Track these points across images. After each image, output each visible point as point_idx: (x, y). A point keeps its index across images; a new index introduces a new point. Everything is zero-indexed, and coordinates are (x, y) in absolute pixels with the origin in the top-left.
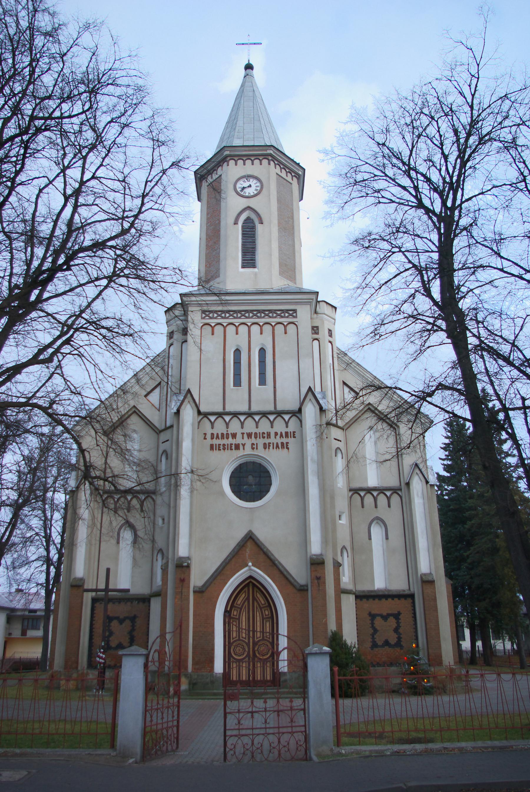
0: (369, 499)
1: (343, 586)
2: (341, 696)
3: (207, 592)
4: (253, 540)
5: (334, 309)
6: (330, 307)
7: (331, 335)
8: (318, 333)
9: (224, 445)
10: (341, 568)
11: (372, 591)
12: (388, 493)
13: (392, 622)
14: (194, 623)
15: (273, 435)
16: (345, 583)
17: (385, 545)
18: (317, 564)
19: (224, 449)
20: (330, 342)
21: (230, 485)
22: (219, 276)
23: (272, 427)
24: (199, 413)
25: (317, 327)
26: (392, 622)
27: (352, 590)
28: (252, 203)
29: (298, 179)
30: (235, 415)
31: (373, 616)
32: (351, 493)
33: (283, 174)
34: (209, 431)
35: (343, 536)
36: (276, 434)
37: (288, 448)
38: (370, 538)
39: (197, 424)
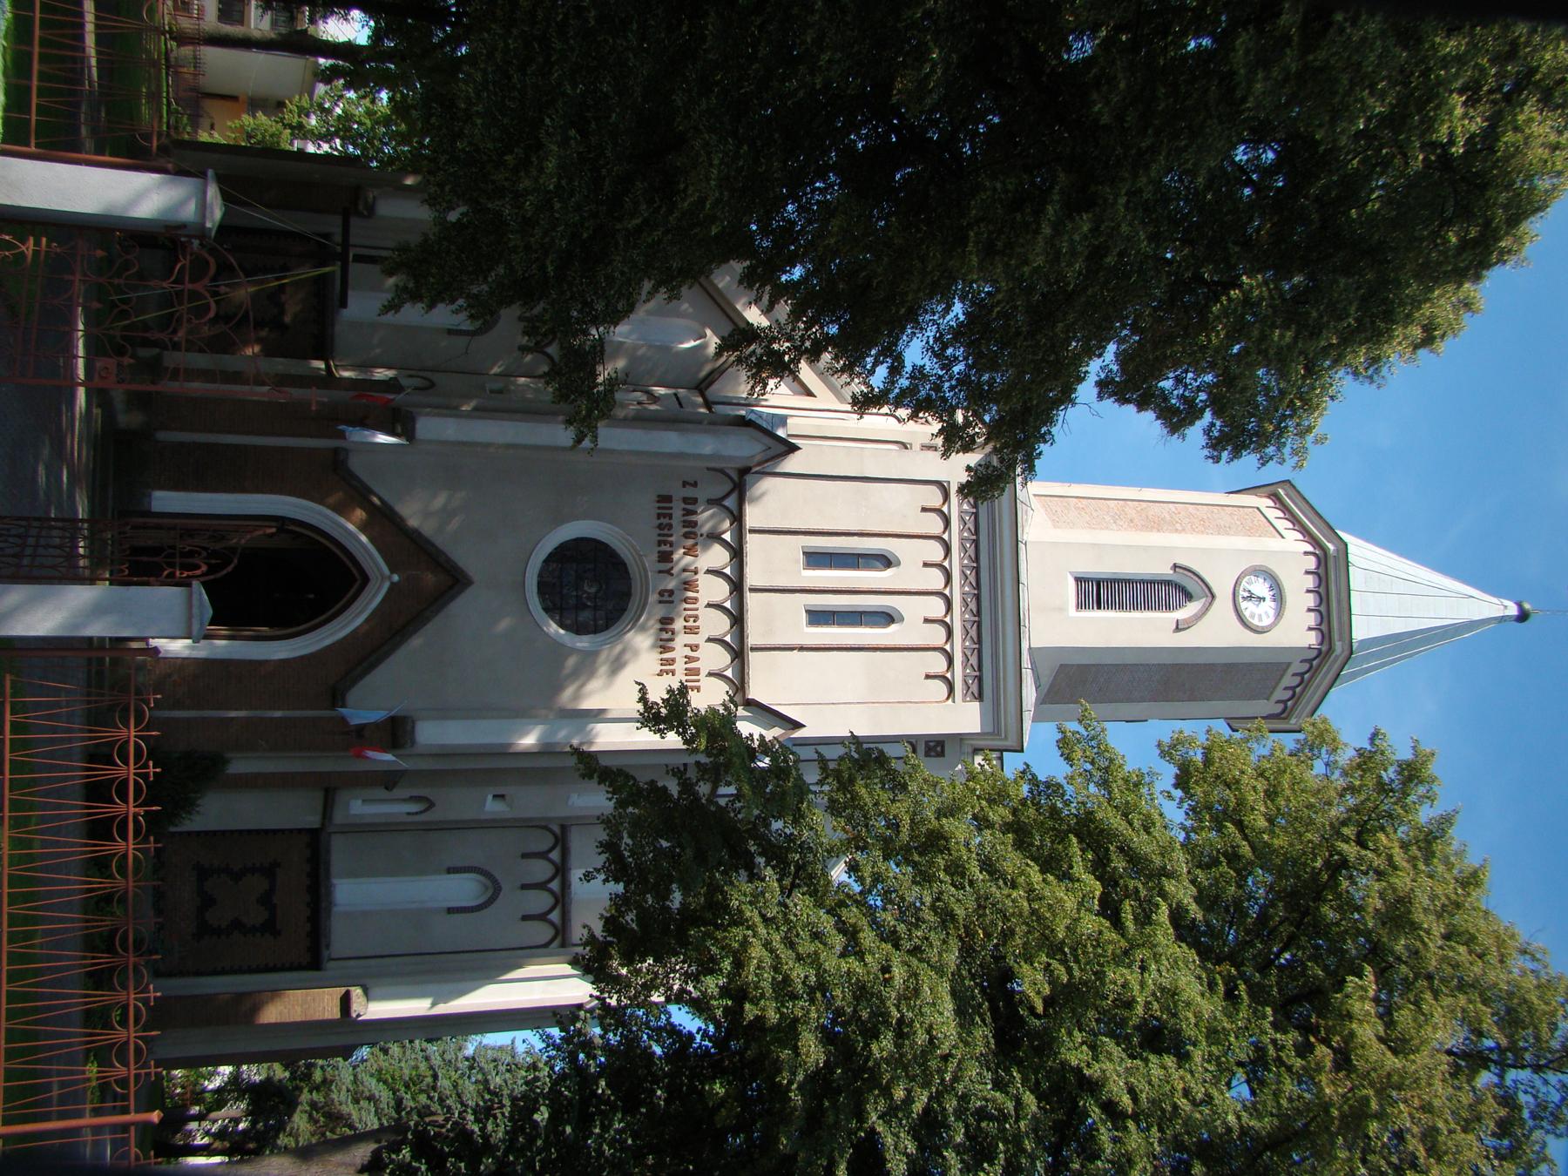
0: (541, 870)
3: (336, 477)
4: (451, 587)
9: (670, 526)
12: (555, 916)
18: (396, 732)
19: (660, 527)
21: (576, 540)
23: (710, 640)
24: (744, 471)
25: (942, 754)
30: (737, 553)
31: (270, 871)
32: (556, 829)
33: (1289, 680)
34: (702, 493)
36: (694, 648)
39: (713, 465)
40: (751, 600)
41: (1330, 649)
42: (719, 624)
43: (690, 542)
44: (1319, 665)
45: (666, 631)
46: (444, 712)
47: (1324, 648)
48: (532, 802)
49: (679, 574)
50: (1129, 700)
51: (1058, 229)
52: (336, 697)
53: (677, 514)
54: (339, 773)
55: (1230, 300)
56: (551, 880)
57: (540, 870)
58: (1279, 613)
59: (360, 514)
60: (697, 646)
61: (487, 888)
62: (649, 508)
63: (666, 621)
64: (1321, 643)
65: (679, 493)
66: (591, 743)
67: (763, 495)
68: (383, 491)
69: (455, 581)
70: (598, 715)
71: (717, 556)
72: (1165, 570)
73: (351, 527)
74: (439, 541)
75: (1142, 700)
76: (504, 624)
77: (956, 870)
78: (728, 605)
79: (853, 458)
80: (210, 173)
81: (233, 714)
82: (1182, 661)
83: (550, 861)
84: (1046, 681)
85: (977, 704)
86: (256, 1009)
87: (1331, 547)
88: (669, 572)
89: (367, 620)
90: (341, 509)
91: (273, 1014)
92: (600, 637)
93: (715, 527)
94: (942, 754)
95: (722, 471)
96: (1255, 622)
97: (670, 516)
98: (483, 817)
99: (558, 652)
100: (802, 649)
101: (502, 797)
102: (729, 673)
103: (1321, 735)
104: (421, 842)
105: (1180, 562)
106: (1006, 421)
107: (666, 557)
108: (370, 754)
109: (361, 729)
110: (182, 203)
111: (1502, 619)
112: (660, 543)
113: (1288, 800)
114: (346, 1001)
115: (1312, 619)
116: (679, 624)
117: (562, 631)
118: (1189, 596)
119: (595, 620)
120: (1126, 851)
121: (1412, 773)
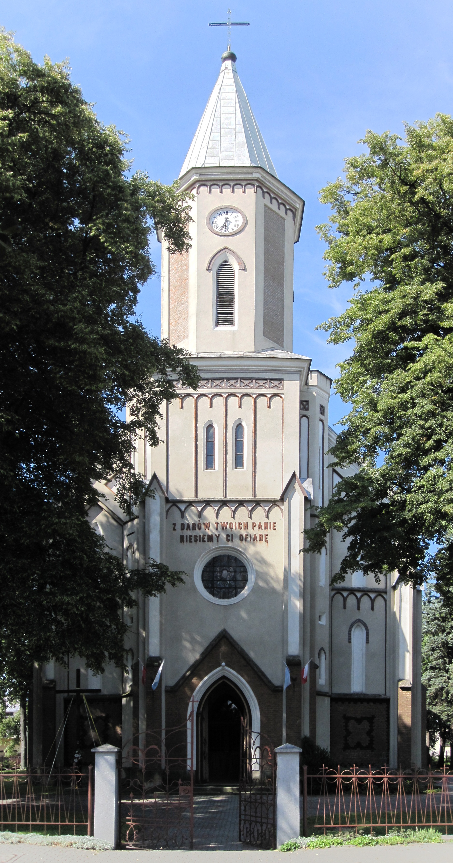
0: (352, 601)
1: (318, 688)
2: (309, 793)
4: (227, 639)
5: (329, 382)
6: (325, 379)
7: (322, 412)
8: (307, 409)
9: (196, 536)
10: (318, 670)
11: (347, 695)
12: (373, 595)
13: (366, 724)
14: (166, 718)
15: (250, 526)
16: (321, 685)
17: (364, 649)
18: (294, 664)
20: (321, 421)
21: (203, 580)
22: (187, 337)
23: (251, 517)
25: (307, 402)
26: (366, 724)
27: (328, 693)
28: (230, 243)
29: (294, 214)
30: (208, 503)
31: (347, 719)
32: (333, 593)
33: (274, 206)
34: (179, 521)
35: (322, 638)
36: (254, 525)
37: (267, 541)
38: (350, 641)
39: (165, 513)
40: (230, 497)
41: (257, 180)
42: (243, 512)
43: (203, 526)
44: (267, 188)
45: (246, 538)
46: (284, 642)
47: (257, 184)
48: (323, 604)
49: (219, 532)
50: (282, 300)
51: (83, 341)
52: (278, 690)
53: (189, 533)
54: (310, 689)
55: (106, 241)
56: (370, 597)
57: (352, 601)
58: (236, 210)
59: (195, 680)
60: (254, 523)
61: (358, 625)
62: (186, 545)
63: (241, 538)
64: (254, 185)
65: (179, 532)
66: (300, 575)
67: (178, 491)
68: (184, 670)
69: (224, 637)
70: (287, 572)
71: (209, 513)
72: (211, 276)
73: (201, 684)
74: (206, 644)
75: (282, 292)
76: (244, 614)
77: (404, 406)
78: (233, 508)
79: (171, 448)
80: (93, 750)
81: (284, 734)
82: (262, 268)
83: (348, 596)
84: (272, 344)
85: (285, 382)
86: (405, 726)
87: (194, 178)
88: (218, 537)
89: (242, 676)
90: (193, 688)
91: (407, 720)
92: (249, 570)
93: (195, 514)
94: (307, 402)
95: (167, 511)
96: (240, 224)
97: (191, 536)
98: (328, 626)
99: (256, 589)
100: (255, 472)
101: (320, 616)
102: (267, 508)
103: (331, 194)
104: (338, 654)
105: (206, 267)
106: (150, 364)
107: (210, 538)
108: (305, 675)
109: (292, 679)
110: (107, 761)
111: (234, 71)
112: (204, 541)
113: (373, 219)
114: (404, 689)
115: (239, 190)
116: (243, 532)
117: (246, 588)
118: (225, 263)
119: (241, 572)
120: (402, 315)
121: (378, 147)
